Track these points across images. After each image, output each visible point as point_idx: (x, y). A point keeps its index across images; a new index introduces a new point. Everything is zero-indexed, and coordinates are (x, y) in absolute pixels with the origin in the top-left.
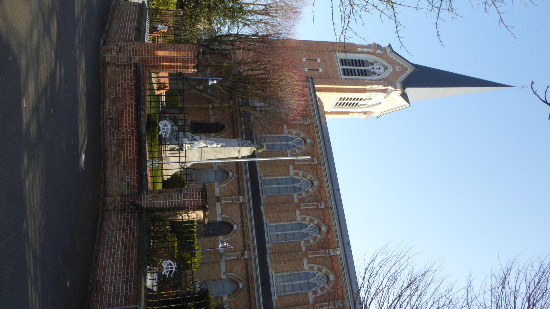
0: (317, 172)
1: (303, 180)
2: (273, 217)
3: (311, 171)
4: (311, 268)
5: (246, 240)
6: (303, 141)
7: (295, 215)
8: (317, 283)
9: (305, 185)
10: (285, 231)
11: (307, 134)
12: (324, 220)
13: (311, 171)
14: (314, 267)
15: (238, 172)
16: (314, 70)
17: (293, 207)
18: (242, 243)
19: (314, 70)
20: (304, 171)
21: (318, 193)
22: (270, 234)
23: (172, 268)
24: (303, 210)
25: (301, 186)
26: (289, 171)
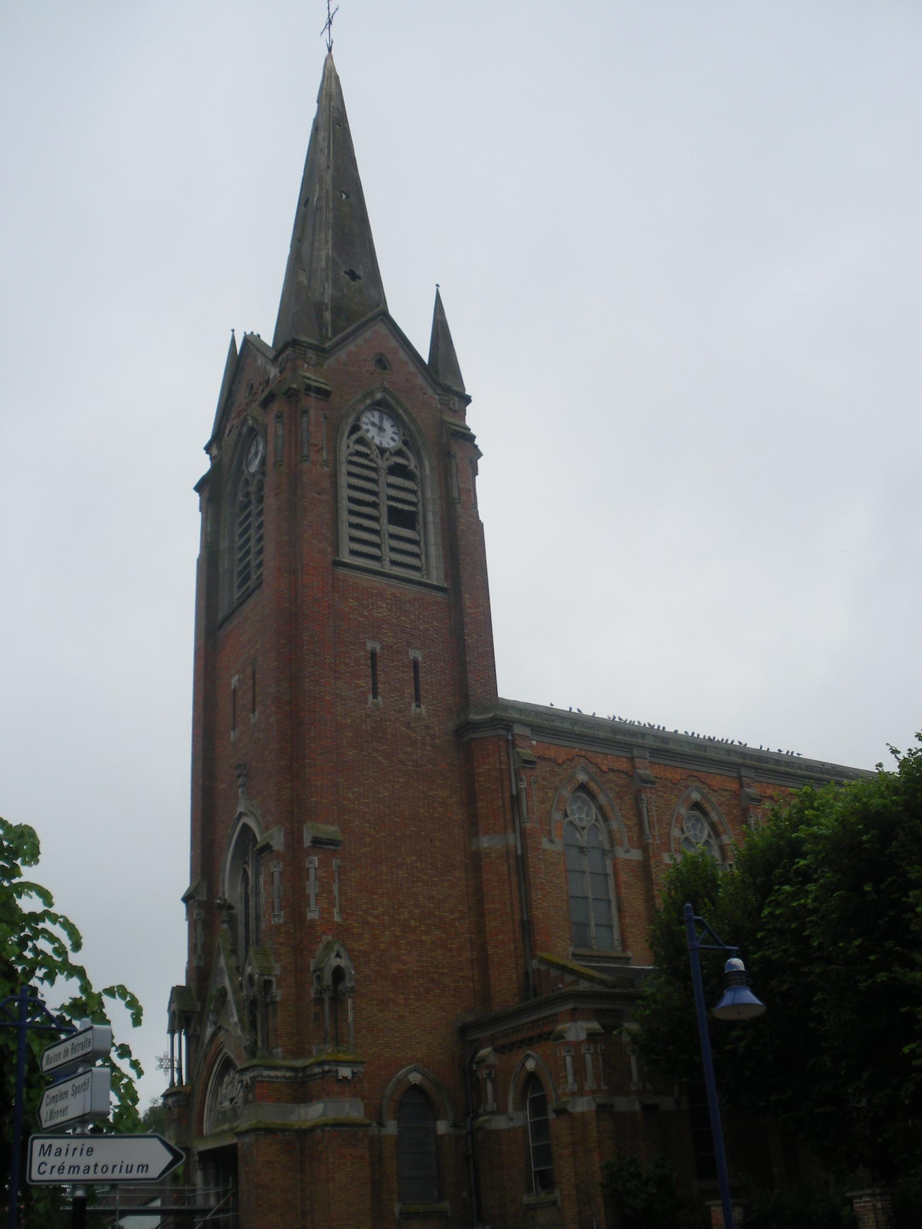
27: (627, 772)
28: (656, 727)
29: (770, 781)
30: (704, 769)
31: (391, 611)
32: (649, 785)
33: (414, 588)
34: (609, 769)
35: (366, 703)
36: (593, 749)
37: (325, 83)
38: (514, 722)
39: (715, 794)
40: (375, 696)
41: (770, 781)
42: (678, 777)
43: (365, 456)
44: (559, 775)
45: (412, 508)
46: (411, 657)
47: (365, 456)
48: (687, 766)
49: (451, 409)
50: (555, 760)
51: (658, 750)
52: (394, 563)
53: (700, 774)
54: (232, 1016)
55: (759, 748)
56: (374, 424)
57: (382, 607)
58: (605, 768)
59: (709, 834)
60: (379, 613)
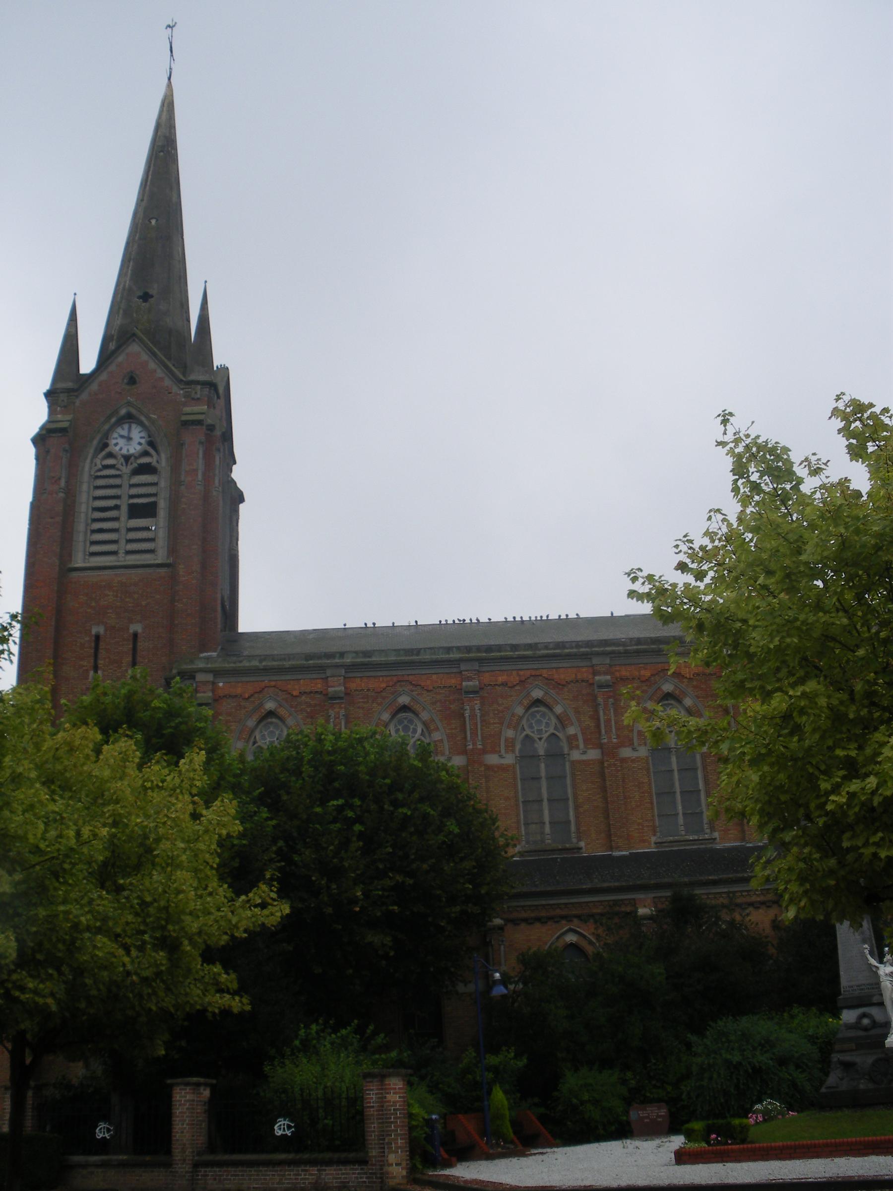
0: (504, 684)
1: (525, 727)
2: (639, 824)
3: (500, 701)
4: (510, 745)
5: (754, 899)
6: (402, 715)
7: (633, 761)
8: (548, 734)
9: (539, 722)
10: (675, 792)
11: (379, 700)
12: (642, 682)
13: (500, 701)
14: (506, 740)
15: (563, 917)
16: (134, 649)
17: (615, 765)
18: (760, 910)
19: (134, 649)
20: (502, 724)
21: (566, 689)
22: (683, 833)
23: (104, 1127)
24: (618, 737)
25: (545, 736)
26: (503, 768)
27: (322, 692)
28: (468, 621)
29: (504, 668)
30: (414, 672)
31: (117, 596)
32: (337, 701)
33: (140, 571)
34: (300, 693)
35: (87, 679)
36: (283, 678)
37: (165, 114)
38: (195, 672)
39: (429, 694)
40: (96, 671)
41: (504, 668)
42: (383, 685)
43: (112, 467)
44: (245, 708)
45: (152, 499)
46: (131, 631)
47: (112, 467)
48: (394, 673)
49: (193, 399)
50: (241, 696)
51: (353, 665)
52: (128, 552)
53: (411, 678)
54: (394, 910)
55: (610, 615)
56: (122, 437)
57: (109, 595)
58: (295, 693)
59: (422, 730)
60: (105, 601)
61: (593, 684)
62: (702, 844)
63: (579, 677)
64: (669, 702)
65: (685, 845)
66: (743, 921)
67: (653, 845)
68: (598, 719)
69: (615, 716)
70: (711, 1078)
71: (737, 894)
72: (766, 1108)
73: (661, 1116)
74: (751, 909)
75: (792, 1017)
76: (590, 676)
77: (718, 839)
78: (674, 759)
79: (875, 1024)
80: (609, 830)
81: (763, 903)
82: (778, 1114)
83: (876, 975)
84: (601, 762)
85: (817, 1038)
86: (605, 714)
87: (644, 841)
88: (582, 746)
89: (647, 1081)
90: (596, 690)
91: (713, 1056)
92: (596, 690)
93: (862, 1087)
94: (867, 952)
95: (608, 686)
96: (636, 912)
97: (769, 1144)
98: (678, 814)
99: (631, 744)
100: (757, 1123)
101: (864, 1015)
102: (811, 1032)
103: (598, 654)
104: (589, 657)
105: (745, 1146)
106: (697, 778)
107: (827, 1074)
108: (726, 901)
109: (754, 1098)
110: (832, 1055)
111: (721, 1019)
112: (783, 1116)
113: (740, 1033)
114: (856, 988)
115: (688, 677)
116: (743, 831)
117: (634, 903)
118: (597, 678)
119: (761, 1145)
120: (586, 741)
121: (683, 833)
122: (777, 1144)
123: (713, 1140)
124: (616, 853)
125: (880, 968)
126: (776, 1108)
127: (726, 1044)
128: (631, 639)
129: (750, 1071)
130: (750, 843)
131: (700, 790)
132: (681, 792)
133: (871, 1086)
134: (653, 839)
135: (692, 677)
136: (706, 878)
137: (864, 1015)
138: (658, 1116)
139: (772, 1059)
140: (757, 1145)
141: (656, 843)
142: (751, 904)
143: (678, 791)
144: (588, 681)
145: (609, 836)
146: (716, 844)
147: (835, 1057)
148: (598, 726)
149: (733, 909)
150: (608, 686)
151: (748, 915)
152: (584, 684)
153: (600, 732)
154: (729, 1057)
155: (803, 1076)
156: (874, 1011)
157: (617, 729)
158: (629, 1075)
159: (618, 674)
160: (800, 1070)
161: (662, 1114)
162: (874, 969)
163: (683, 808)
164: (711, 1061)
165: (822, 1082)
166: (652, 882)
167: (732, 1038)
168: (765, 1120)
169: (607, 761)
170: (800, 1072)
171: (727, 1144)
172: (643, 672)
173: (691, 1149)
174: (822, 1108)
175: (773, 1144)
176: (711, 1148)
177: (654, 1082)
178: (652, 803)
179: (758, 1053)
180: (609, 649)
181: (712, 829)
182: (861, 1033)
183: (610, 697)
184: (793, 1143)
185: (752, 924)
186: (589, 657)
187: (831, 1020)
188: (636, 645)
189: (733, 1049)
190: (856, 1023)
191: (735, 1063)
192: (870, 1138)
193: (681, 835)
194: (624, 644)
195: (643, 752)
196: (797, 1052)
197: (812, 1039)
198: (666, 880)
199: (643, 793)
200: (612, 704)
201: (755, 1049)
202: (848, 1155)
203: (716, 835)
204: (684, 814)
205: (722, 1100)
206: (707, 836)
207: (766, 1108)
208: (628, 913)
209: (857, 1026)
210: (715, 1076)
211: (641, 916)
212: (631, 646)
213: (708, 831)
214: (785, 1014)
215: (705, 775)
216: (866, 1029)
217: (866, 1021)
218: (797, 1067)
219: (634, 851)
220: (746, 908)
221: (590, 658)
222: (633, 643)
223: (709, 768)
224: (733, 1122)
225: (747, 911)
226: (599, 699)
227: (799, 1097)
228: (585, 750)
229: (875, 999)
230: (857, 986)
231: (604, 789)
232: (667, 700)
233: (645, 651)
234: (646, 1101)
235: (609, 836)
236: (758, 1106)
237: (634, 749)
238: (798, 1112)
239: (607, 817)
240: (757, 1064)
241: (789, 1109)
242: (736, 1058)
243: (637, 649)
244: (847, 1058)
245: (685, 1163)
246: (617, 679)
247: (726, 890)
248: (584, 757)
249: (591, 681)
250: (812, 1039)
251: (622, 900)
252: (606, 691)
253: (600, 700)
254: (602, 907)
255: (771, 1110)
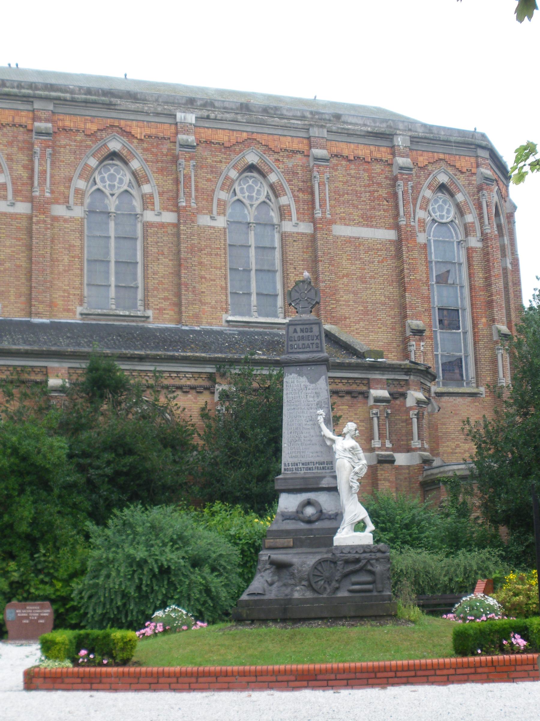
2: (64, 291)
5: (183, 382)
7: (66, 221)
17: (45, 221)
18: (189, 396)
24: (52, 192)
61: (32, 131)
62: (133, 321)
63: (17, 120)
64: (114, 162)
65: (114, 320)
66: (168, 404)
67: (78, 316)
68: (32, 170)
69: (52, 169)
70: (108, 576)
71: (164, 375)
72: (169, 616)
73: (43, 617)
74: (179, 392)
75: (213, 514)
76: (30, 122)
77: (151, 318)
78: (112, 224)
79: (321, 515)
80: (30, 294)
81: (193, 388)
82: (183, 624)
83: (330, 450)
84: (30, 218)
85: (240, 540)
86: (40, 164)
87: (68, 310)
88: (10, 196)
89: (32, 575)
90: (34, 137)
91: (113, 549)
92: (34, 137)
93: (296, 595)
94: (321, 419)
95: (48, 134)
96: (46, 382)
97: (161, 669)
98: (110, 286)
99: (66, 201)
100: (155, 634)
101: (309, 503)
102: (232, 533)
103: (40, 98)
104: (31, 99)
105: (126, 669)
106: (135, 250)
107: (248, 581)
108: (151, 382)
109: (158, 603)
110: (261, 553)
111: (128, 507)
112: (189, 627)
113: (149, 525)
114: (301, 466)
115: (139, 137)
116: (180, 313)
117: (45, 372)
118: (37, 124)
119: (149, 669)
120: (16, 192)
121: (113, 307)
122: (172, 669)
123: (83, 657)
124: (36, 320)
125: (337, 442)
126: (181, 616)
127: (131, 536)
128: (80, 88)
129: (156, 570)
130: (187, 325)
131: (137, 263)
132: (117, 262)
133: (309, 595)
134: (79, 309)
135: (143, 138)
136: (132, 352)
137: (309, 503)
138: (40, 617)
139: (183, 558)
140: (144, 669)
141: (82, 314)
142: (180, 388)
143: (113, 259)
144: (26, 126)
145: (30, 298)
146: (149, 323)
147: (264, 555)
148: (31, 178)
149: (158, 391)
150: (48, 134)
151: (174, 398)
152: (21, 129)
153: (32, 185)
154: (132, 551)
155: (219, 580)
156: (322, 498)
157: (52, 184)
158: (12, 565)
159: (60, 124)
160: (216, 573)
161: (45, 615)
162: (328, 443)
163: (117, 279)
164: (111, 556)
165: (241, 591)
166: (69, 350)
167: (139, 529)
168: (165, 631)
169: (36, 216)
170: (216, 576)
171: (101, 665)
172: (89, 125)
173: (49, 669)
174: (239, 620)
175: (167, 669)
176: (76, 669)
177: (41, 576)
178: (82, 270)
179: (168, 549)
180: (54, 94)
181: (146, 306)
182: (302, 526)
183: (48, 147)
184: (195, 669)
185: (178, 408)
186: (31, 99)
187: (256, 520)
188: (85, 94)
189: (138, 543)
190: (297, 512)
191: (138, 560)
192: (306, 666)
193: (111, 309)
194: (72, 92)
195: (78, 212)
196: (214, 552)
197: (234, 540)
198: (86, 349)
199: (73, 257)
200: (50, 154)
201: (165, 544)
202: (271, 688)
203: (150, 313)
204: (117, 286)
205: (119, 603)
206: (139, 314)
207: (169, 616)
208: (37, 383)
209: (297, 516)
210: (114, 574)
211: (52, 387)
212: (80, 94)
213: (142, 308)
214: (206, 510)
215: (144, 247)
216: (309, 521)
217: (310, 511)
218: (213, 569)
219: (56, 320)
220: (174, 392)
221: (32, 102)
222: (82, 91)
223: (150, 239)
224: (113, 635)
225: (175, 394)
226: (36, 147)
227: (212, 605)
228: (14, 201)
229: (324, 483)
230: (303, 464)
231: (30, 248)
232: (113, 160)
233: (95, 102)
234: (30, 598)
235: (30, 298)
236: (159, 614)
237: (69, 208)
238: (209, 623)
239: (30, 279)
240: (165, 563)
241: (197, 619)
242: (141, 553)
243: (86, 99)
244: (280, 556)
245: (36, 689)
246: (58, 129)
247: (152, 368)
248: (11, 210)
249: (29, 127)
250: (234, 540)
251: (32, 367)
252: (45, 140)
253: (37, 148)
254: (8, 373)
255: (175, 619)
